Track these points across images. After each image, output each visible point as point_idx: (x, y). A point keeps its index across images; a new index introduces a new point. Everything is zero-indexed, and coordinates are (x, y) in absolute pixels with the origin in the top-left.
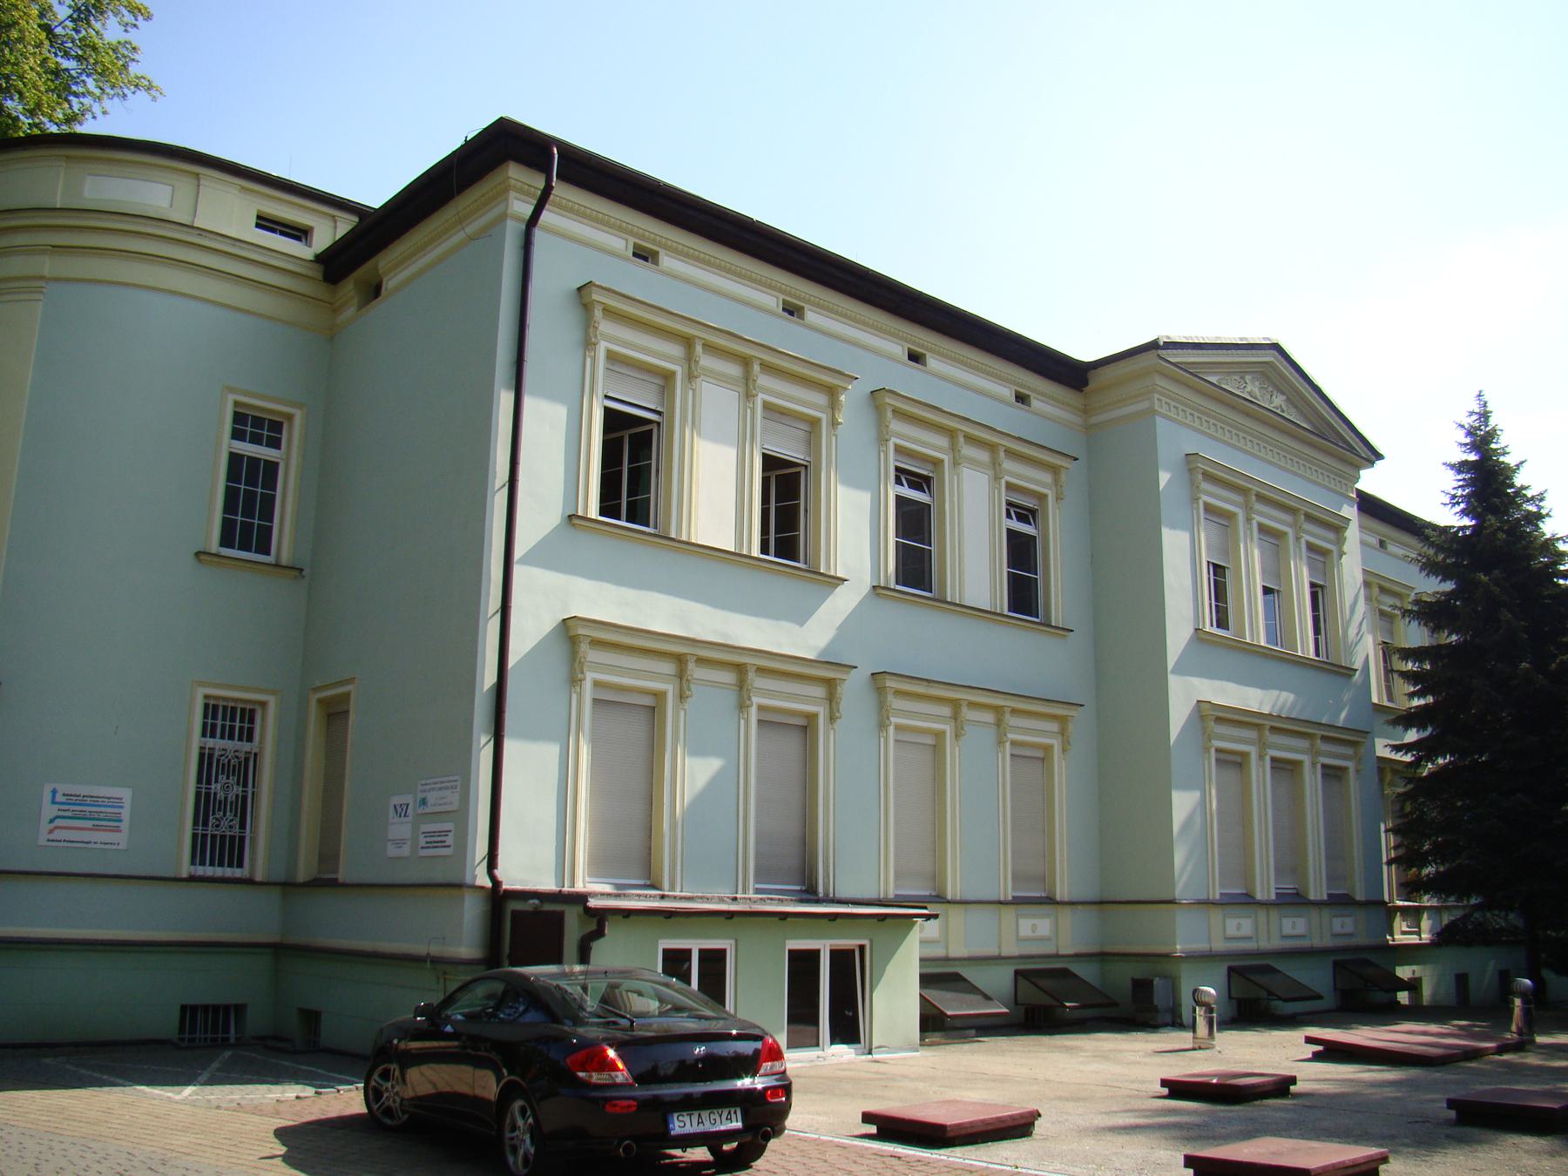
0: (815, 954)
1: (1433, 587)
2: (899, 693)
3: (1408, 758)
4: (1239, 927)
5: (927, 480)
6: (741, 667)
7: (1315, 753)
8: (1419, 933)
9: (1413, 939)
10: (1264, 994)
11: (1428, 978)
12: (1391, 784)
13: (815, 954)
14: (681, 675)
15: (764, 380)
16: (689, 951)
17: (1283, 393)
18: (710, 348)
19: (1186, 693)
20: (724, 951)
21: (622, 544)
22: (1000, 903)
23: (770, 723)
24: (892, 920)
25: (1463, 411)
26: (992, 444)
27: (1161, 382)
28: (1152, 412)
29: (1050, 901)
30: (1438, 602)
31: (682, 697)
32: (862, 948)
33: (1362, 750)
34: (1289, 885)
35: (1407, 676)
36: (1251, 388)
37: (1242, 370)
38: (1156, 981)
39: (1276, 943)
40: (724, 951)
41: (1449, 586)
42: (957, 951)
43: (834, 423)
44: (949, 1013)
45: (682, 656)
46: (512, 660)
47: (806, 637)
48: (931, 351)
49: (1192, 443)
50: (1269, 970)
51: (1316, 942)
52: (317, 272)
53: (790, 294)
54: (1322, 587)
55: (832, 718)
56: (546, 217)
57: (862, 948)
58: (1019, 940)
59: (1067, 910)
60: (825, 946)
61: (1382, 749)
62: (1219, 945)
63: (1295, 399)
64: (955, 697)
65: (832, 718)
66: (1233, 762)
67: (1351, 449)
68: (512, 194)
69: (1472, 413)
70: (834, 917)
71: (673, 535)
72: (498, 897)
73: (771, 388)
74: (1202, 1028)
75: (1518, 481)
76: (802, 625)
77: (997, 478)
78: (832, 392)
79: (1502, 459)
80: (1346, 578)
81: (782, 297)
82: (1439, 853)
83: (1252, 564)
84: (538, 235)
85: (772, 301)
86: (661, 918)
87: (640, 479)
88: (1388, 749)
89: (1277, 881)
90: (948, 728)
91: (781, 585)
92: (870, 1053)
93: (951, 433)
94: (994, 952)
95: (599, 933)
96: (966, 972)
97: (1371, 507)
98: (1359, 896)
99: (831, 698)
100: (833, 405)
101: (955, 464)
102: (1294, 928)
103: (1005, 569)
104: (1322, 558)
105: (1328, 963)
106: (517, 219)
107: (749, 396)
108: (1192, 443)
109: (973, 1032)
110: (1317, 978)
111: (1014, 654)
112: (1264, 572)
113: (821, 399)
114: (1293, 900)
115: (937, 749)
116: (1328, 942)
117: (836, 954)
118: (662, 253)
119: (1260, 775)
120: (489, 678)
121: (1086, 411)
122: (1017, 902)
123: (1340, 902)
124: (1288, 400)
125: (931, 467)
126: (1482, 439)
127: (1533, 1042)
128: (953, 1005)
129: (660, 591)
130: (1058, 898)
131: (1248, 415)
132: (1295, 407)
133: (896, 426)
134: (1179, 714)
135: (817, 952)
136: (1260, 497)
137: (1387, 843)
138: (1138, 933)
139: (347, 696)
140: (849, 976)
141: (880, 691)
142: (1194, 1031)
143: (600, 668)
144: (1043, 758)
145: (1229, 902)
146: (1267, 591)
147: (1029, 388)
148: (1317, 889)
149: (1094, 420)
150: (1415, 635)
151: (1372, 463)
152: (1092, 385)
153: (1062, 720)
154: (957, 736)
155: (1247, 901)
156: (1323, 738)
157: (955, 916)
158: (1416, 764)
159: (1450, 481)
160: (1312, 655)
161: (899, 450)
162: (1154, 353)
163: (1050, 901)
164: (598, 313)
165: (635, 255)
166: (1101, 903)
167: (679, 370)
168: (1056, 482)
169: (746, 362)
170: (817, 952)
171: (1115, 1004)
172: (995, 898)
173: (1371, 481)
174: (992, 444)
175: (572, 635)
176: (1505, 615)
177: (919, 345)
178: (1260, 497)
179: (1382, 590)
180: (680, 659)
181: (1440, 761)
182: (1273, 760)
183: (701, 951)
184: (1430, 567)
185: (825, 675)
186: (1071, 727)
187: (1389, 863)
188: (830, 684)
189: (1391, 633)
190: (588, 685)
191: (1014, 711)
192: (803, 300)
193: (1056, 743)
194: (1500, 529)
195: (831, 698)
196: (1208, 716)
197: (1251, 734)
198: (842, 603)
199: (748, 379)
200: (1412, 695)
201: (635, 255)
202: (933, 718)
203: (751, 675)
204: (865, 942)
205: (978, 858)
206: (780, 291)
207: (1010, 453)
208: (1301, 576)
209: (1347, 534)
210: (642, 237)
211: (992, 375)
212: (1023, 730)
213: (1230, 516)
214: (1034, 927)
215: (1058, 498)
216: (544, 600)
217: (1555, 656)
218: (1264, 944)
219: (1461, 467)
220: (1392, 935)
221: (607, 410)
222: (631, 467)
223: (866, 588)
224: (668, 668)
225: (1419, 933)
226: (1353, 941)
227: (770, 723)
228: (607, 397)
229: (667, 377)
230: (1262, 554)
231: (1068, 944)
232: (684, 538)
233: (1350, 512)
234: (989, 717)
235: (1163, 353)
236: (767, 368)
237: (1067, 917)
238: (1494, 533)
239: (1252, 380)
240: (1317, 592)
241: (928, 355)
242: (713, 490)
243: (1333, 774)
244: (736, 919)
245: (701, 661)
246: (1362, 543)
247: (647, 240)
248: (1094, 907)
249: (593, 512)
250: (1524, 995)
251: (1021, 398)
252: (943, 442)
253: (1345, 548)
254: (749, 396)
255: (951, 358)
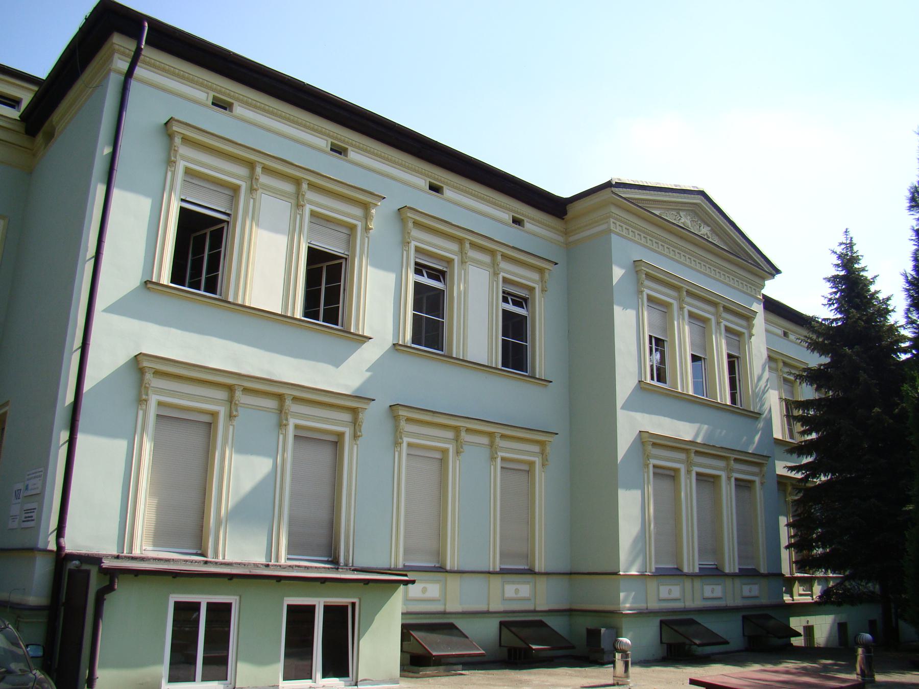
0: (311, 609)
1: (816, 360)
2: (409, 420)
3: (799, 476)
4: (670, 592)
5: (443, 273)
6: (280, 396)
7: (730, 470)
8: (811, 595)
9: (808, 599)
10: (687, 642)
11: (823, 627)
12: (791, 494)
13: (311, 609)
14: (231, 401)
15: (310, 195)
16: (199, 604)
17: (708, 226)
18: (267, 170)
19: (630, 425)
20: (230, 605)
21: (193, 303)
22: (489, 573)
23: (303, 437)
24: (384, 583)
25: (835, 242)
26: (489, 249)
27: (614, 210)
28: (610, 231)
29: (531, 572)
30: (819, 369)
31: (231, 416)
32: (353, 604)
33: (765, 469)
34: (710, 562)
35: (803, 420)
36: (685, 220)
37: (678, 207)
38: (603, 630)
39: (698, 603)
40: (230, 605)
41: (826, 360)
42: (452, 607)
43: (367, 229)
44: (434, 653)
45: (232, 386)
46: (87, 386)
47: (346, 375)
48: (447, 184)
49: (638, 253)
50: (692, 622)
51: (730, 603)
52: (21, 128)
53: (336, 139)
54: (738, 358)
55: (355, 436)
56: (139, 71)
57: (353, 604)
58: (504, 599)
59: (543, 579)
60: (319, 603)
61: (781, 468)
62: (654, 605)
63: (717, 229)
64: (457, 425)
65: (355, 436)
66: (666, 475)
67: (757, 265)
68: (116, 56)
69: (841, 244)
70: (367, 582)
71: (231, 299)
72: (61, 558)
73: (315, 201)
74: (620, 665)
75: (872, 288)
76: (337, 366)
77: (496, 274)
78: (366, 207)
79: (862, 274)
80: (754, 351)
81: (330, 140)
82: (823, 541)
83: (684, 339)
84: (134, 85)
85: (323, 143)
86: (170, 578)
87: (334, 295)
88: (786, 470)
89: (700, 559)
90: (451, 448)
91: (319, 337)
92: (356, 685)
93: (460, 241)
94: (484, 608)
95: (110, 588)
96: (460, 624)
97: (773, 307)
98: (763, 570)
99: (355, 423)
100: (367, 217)
101: (463, 262)
102: (713, 593)
103: (500, 337)
104: (737, 337)
105: (739, 617)
106: (119, 72)
107: (299, 206)
108: (638, 253)
109: (460, 667)
110: (730, 630)
111: (506, 397)
112: (692, 344)
113: (358, 212)
114: (713, 573)
115: (443, 462)
116: (739, 602)
117: (328, 609)
118: (236, 104)
119: (688, 487)
120: (70, 398)
121: (566, 233)
122: (503, 572)
123: (748, 574)
124: (712, 230)
125: (445, 264)
126: (848, 261)
127: (873, 681)
128: (438, 646)
129: (215, 336)
130: (537, 570)
131: (681, 238)
132: (717, 235)
133: (415, 233)
134: (625, 440)
135: (313, 607)
136: (689, 293)
137: (785, 535)
138: (592, 596)
139: (5, 413)
140: (340, 623)
141: (396, 418)
142: (614, 667)
143: (160, 393)
144: (529, 471)
145: (661, 574)
146: (695, 358)
147: (523, 215)
148: (731, 565)
149: (571, 239)
150: (807, 392)
151: (773, 276)
152: (570, 214)
153: (541, 443)
154: (458, 453)
155: (676, 573)
156: (736, 460)
157: (453, 582)
158: (805, 480)
159: (827, 289)
160: (729, 403)
161: (418, 250)
162: (608, 190)
163: (531, 572)
164: (178, 140)
165: (213, 104)
166: (571, 574)
167: (244, 186)
168: (542, 279)
169: (251, 165)
170: (313, 607)
171: (573, 647)
172: (486, 569)
173: (773, 289)
174: (489, 249)
175: (140, 367)
176: (863, 376)
177: (437, 180)
178: (689, 293)
179: (785, 364)
180: (230, 389)
181: (823, 478)
182: (698, 474)
183: (209, 604)
184: (814, 347)
185: (353, 406)
186: (548, 449)
187: (787, 547)
188: (354, 411)
189: (792, 393)
190: (404, 445)
191: (503, 436)
192: (347, 143)
193: (537, 460)
194: (859, 318)
195: (355, 423)
196: (647, 442)
197: (682, 456)
198: (369, 354)
199: (298, 195)
200: (803, 433)
201: (213, 104)
202: (440, 439)
203: (288, 402)
204: (356, 600)
205: (473, 537)
206: (329, 136)
207: (505, 257)
208: (720, 348)
209: (755, 322)
210: (220, 92)
211: (495, 204)
212: (509, 450)
213: (667, 305)
214: (517, 591)
215: (543, 290)
216: (116, 339)
217: (898, 404)
218: (690, 604)
219: (834, 280)
220: (792, 596)
221: (182, 210)
222: (201, 253)
223: (390, 344)
224: (222, 395)
225: (811, 595)
226: (757, 602)
227: (303, 437)
228: (183, 200)
229: (235, 190)
230: (691, 332)
231: (543, 604)
232: (240, 302)
233: (758, 308)
234: (485, 440)
235: (616, 190)
236: (312, 186)
237: (543, 584)
238: (855, 322)
239: (685, 216)
240: (733, 363)
241: (445, 187)
242: (266, 265)
243: (743, 485)
244: (235, 580)
245: (246, 390)
246: (767, 331)
247: (224, 94)
248: (568, 577)
249: (166, 279)
250: (867, 647)
251: (517, 221)
252: (454, 247)
253: (754, 331)
254: (299, 206)
255: (462, 190)
